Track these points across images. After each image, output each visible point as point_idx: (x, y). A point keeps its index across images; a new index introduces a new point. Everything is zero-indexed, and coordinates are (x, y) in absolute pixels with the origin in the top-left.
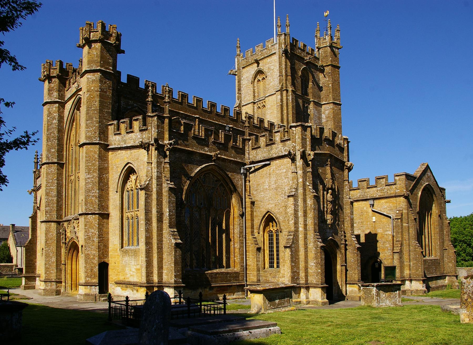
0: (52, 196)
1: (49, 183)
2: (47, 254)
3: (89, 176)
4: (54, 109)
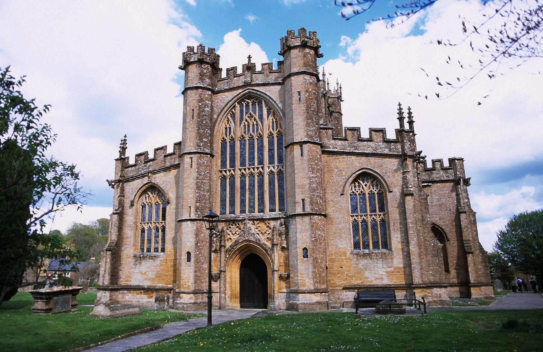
0: (204, 191)
1: (200, 175)
2: (197, 259)
3: (313, 175)
4: (207, 96)
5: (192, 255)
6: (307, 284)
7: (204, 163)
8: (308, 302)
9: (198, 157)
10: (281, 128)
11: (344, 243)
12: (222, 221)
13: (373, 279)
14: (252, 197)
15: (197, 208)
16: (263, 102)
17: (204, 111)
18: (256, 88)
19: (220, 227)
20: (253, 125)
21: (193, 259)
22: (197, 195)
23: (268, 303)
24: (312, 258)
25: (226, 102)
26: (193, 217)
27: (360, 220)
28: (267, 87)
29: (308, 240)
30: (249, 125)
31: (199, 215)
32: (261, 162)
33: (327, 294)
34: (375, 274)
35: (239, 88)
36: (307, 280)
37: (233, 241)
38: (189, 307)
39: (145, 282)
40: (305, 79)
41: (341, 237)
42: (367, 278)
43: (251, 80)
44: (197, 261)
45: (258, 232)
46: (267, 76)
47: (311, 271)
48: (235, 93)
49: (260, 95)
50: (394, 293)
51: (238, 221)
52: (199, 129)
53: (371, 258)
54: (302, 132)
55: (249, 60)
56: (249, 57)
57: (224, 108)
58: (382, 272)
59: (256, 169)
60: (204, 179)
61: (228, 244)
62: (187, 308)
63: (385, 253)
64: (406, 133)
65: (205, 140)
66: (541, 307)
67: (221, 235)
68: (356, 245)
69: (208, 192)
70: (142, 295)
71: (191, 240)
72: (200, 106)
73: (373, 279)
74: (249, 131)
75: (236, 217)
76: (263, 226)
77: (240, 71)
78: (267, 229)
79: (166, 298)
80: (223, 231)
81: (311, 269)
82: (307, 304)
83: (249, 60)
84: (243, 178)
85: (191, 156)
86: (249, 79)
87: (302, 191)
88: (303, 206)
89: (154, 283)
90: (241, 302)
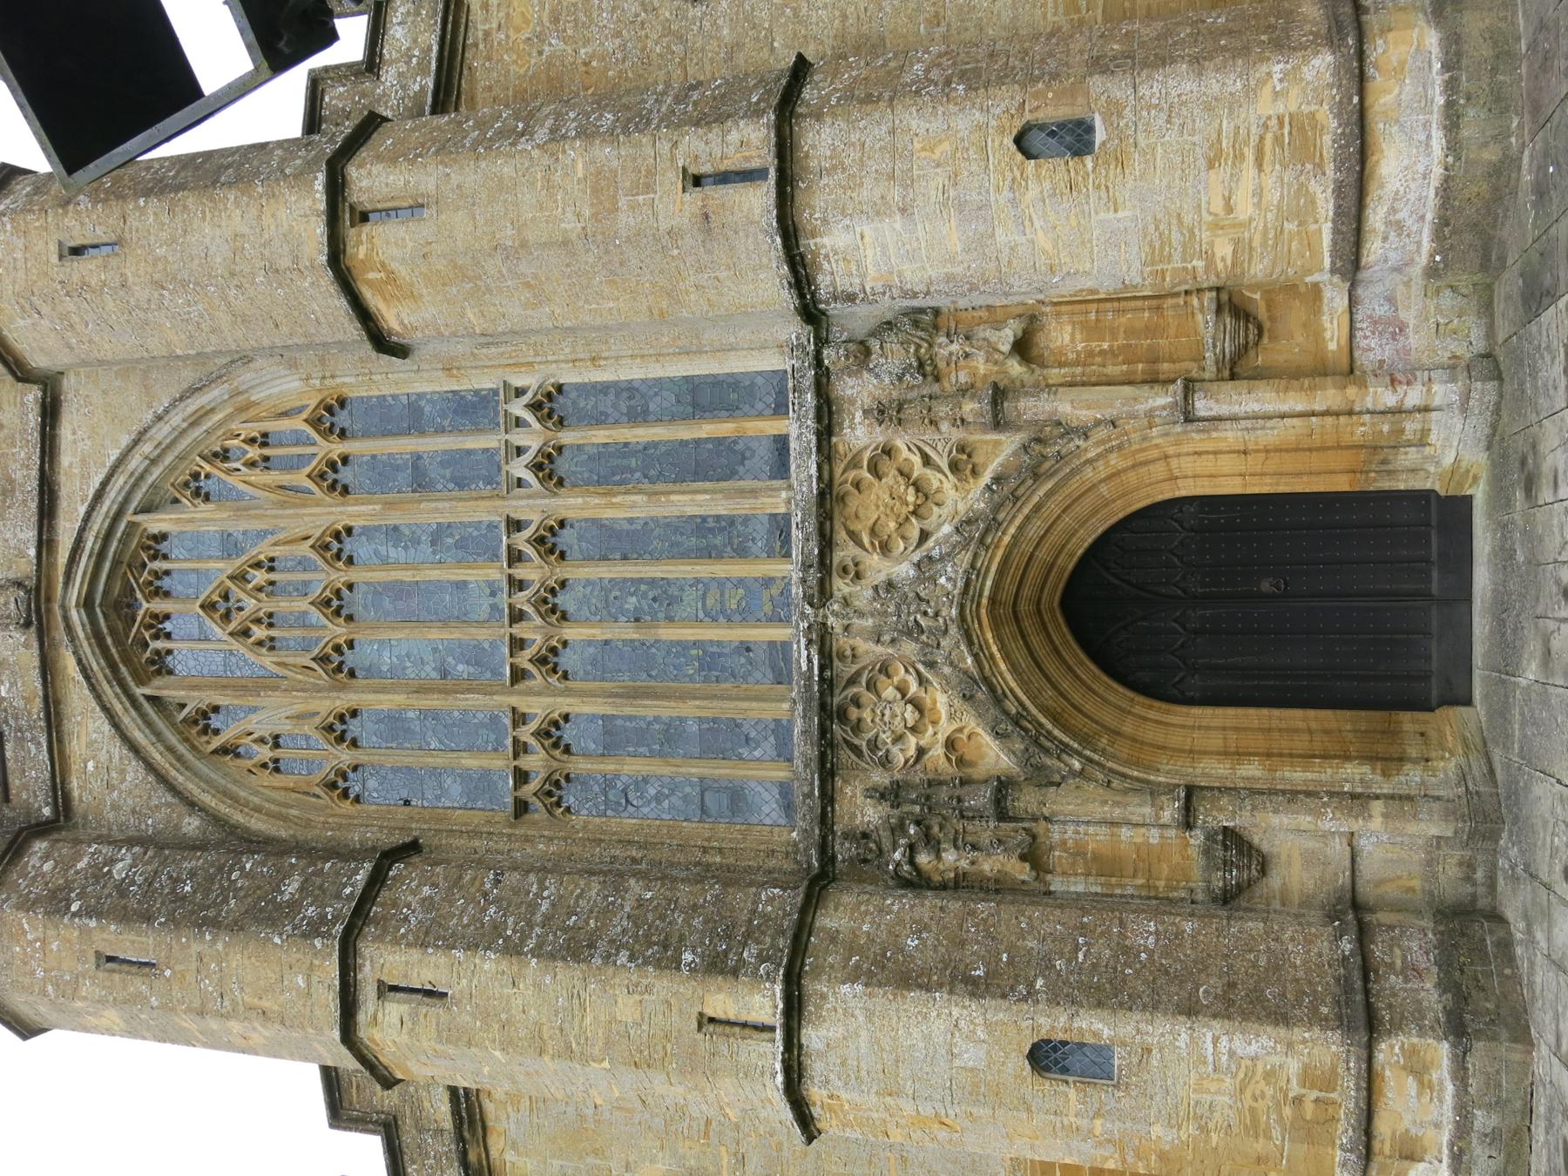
0: (606, 912)
1: (497, 928)
2: (1088, 989)
5: (1054, 1023)
6: (1293, 102)
7: (428, 904)
8: (1437, 79)
9: (379, 939)
10: (300, 410)
14: (690, 595)
15: (718, 966)
16: (155, 523)
17: (122, 890)
19: (871, 814)
21: (1093, 1025)
22: (623, 958)
23: (1426, 496)
24: (1096, 83)
25: (118, 750)
26: (765, 1004)
28: (64, 492)
29: (965, 121)
31: (762, 958)
36: (1266, 107)
37: (971, 723)
38: (1492, 1083)
44: (1107, 993)
45: (915, 534)
47: (1189, 86)
48: (77, 697)
51: (828, 685)
52: (214, 924)
54: (283, 214)
57: (150, 767)
59: (520, 572)
60: (533, 907)
61: (994, 755)
62: (1499, 1105)
65: (291, 887)
67: (926, 805)
69: (620, 889)
71: (939, 1027)
72: (88, 912)
75: (807, 702)
76: (874, 503)
80: (892, 794)
81: (1178, 83)
82: (1451, 86)
84: (566, 538)
85: (368, 993)
87: (634, 190)
88: (724, 178)
90: (1422, 705)
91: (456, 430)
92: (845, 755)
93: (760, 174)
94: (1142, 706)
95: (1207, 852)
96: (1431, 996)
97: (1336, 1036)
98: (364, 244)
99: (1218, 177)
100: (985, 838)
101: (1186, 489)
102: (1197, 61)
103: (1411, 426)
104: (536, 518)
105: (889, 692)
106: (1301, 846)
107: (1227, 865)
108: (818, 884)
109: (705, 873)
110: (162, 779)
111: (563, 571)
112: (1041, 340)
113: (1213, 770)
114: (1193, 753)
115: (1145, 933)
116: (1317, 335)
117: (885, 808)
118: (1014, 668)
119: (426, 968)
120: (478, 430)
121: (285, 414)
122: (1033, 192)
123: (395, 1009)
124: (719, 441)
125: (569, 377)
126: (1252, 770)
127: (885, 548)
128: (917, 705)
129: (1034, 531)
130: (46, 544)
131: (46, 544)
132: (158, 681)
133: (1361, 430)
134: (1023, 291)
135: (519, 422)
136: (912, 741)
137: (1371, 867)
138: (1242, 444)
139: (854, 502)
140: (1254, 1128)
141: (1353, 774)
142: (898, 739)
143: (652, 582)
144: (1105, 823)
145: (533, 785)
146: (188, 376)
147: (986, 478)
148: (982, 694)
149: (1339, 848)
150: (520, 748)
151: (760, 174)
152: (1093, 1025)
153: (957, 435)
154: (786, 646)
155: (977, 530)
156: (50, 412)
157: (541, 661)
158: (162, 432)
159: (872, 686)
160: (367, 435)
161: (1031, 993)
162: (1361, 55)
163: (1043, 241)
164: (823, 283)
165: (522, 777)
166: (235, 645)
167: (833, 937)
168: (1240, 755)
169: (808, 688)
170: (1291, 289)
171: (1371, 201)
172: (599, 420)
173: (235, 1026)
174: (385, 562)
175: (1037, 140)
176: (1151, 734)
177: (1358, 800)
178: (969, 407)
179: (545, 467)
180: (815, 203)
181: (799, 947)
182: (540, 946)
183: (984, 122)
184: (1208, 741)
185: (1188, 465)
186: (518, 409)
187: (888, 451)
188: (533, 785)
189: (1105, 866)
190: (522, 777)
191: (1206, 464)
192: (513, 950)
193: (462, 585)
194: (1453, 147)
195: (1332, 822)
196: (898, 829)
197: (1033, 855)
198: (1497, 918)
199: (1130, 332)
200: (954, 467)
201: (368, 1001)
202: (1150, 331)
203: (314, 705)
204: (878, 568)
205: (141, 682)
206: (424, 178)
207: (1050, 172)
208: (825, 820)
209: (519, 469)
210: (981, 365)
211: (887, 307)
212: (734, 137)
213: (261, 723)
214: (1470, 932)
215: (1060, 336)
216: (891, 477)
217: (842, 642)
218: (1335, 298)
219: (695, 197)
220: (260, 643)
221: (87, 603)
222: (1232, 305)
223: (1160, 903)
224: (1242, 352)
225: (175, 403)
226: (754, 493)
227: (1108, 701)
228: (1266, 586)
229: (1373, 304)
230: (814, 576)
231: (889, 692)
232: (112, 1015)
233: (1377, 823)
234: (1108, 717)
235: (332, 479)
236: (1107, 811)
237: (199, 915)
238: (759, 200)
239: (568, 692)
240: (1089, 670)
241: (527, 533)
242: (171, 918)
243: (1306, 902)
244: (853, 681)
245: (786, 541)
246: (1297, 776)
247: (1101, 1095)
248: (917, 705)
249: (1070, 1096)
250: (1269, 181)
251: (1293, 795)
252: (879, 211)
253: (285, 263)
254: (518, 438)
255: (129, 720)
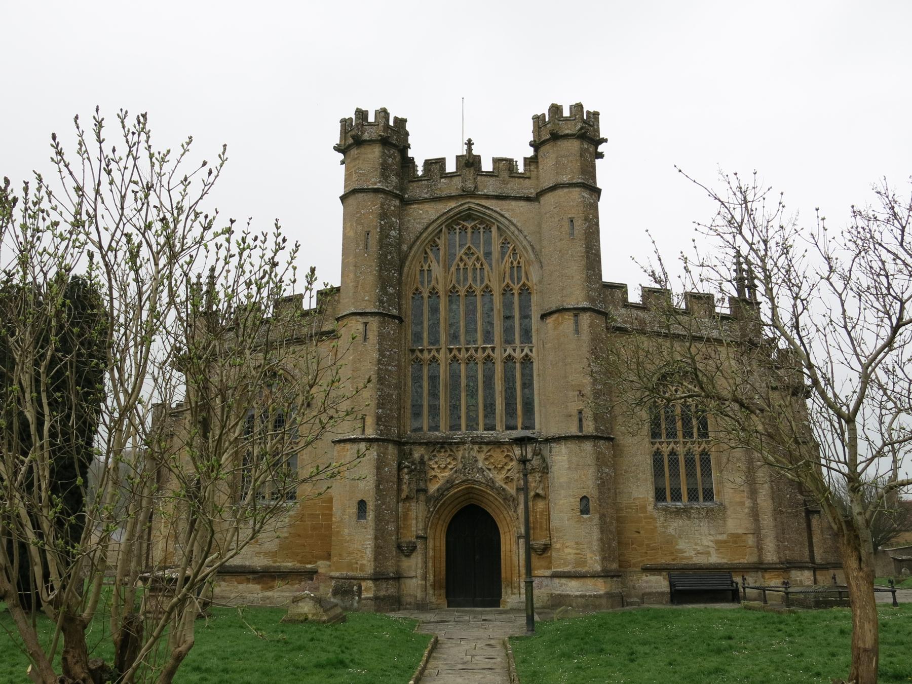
0: (389, 386)
5: (371, 506)
8: (592, 594)
9: (380, 322)
10: (528, 279)
11: (640, 490)
12: (420, 444)
13: (693, 554)
14: (473, 402)
15: (379, 419)
16: (494, 229)
17: (388, 236)
18: (484, 202)
20: (475, 269)
21: (371, 515)
22: (379, 393)
24: (597, 516)
25: (426, 222)
26: (370, 433)
27: (666, 450)
30: (465, 269)
32: (488, 336)
33: (619, 579)
34: (696, 544)
35: (450, 198)
36: (589, 555)
37: (441, 482)
39: (255, 559)
40: (584, 197)
41: (638, 479)
42: (683, 552)
43: (476, 187)
44: (378, 519)
45: (490, 467)
46: (505, 182)
49: (490, 216)
50: (731, 577)
51: (450, 444)
52: (381, 269)
53: (689, 518)
54: (578, 292)
55: (470, 150)
56: (470, 143)
57: (421, 234)
58: (707, 541)
59: (480, 351)
61: (433, 488)
63: (712, 510)
64: (744, 304)
65: (391, 290)
66: (910, 600)
67: (420, 471)
68: (660, 495)
70: (250, 585)
72: (381, 227)
73: (693, 554)
74: (466, 279)
75: (445, 438)
76: (498, 456)
77: (451, 167)
78: (507, 460)
79: (355, 588)
80: (422, 462)
81: (596, 534)
82: (590, 596)
83: (470, 150)
84: (490, 365)
85: (365, 319)
86: (470, 185)
88: (580, 420)
89: (275, 562)
91: (521, 330)
92: (431, 449)
93: (581, 431)
94: (446, 525)
95: (410, 542)
96: (382, 593)
97: (372, 571)
98: (569, 318)
99: (572, 544)
100: (412, 486)
101: (502, 536)
102: (601, 539)
103: (516, 591)
104: (495, 356)
105: (448, 460)
106: (414, 565)
107: (408, 547)
108: (399, 444)
109: (399, 414)
110: (418, 238)
111: (480, 363)
112: (540, 500)
113: (431, 544)
114: (434, 539)
115: (391, 527)
116: (539, 569)
117: (418, 460)
118: (455, 493)
119: (373, 337)
120: (521, 336)
121: (527, 274)
122: (572, 500)
123: (361, 327)
124: (516, 410)
125: (535, 366)
126: (431, 553)
127: (486, 459)
128: (446, 467)
129: (490, 498)
130: (487, 197)
131: (487, 197)
132: (446, 231)
133: (515, 579)
134: (551, 496)
135: (522, 351)
136: (436, 466)
137: (408, 581)
138: (512, 550)
139: (498, 450)
140: (350, 553)
141: (431, 577)
142: (436, 463)
143: (477, 390)
144: (417, 517)
145: (419, 355)
146: (537, 247)
147: (504, 486)
148: (449, 485)
149: (413, 574)
150: (430, 351)
151: (581, 431)
152: (371, 515)
153: (515, 478)
154: (460, 429)
155: (491, 483)
156: (528, 199)
157: (455, 357)
158: (521, 238)
159: (450, 455)
160: (520, 301)
161: (377, 500)
162: (599, 577)
163: (561, 502)
164: (554, 445)
165: (422, 351)
166: (458, 258)
167: (387, 449)
168: (434, 550)
169: (449, 438)
170: (550, 562)
171: (568, 580)
172: (523, 375)
173: (352, 276)
174: (483, 306)
175: (584, 502)
176: (439, 528)
177: (425, 578)
178: (522, 482)
179: (510, 358)
180: (573, 446)
181: (383, 441)
182: (381, 369)
183: (591, 490)
184: (438, 542)
185: (508, 538)
186: (526, 350)
187: (512, 460)
188: (419, 355)
189: (406, 517)
190: (422, 351)
191: (508, 542)
192: (379, 362)
193: (476, 331)
194: (576, 597)
195: (420, 572)
196: (413, 463)
197: (408, 498)
198: (399, 610)
199: (541, 523)
200: (507, 478)
201: (362, 319)
202: (541, 527)
203: (440, 284)
204: (481, 457)
205: (446, 226)
206: (585, 336)
207: (576, 504)
208: (414, 443)
209: (509, 351)
210: (533, 485)
211: (548, 460)
212: (590, 423)
213: (434, 266)
214: (396, 602)
215: (541, 505)
216: (505, 460)
217: (462, 448)
218: (548, 573)
219: (575, 412)
220: (458, 265)
221: (470, 209)
222: (547, 548)
223: (398, 529)
224: (535, 550)
225: (529, 242)
226: (501, 421)
227: (447, 517)
228: (477, 557)
229: (546, 582)
230: (479, 440)
231: (448, 460)
232: (351, 234)
233: (420, 582)
234: (443, 517)
235: (507, 291)
236: (420, 515)
237: (383, 263)
238: (574, 430)
239: (446, 365)
240: (455, 511)
241: (491, 353)
242: (382, 255)
243: (399, 566)
244: (451, 450)
245: (488, 429)
246: (430, 564)
247: (355, 517)
248: (446, 467)
249: (354, 510)
250: (572, 556)
251: (426, 563)
252: (570, 462)
253: (565, 293)
254: (518, 350)
255: (435, 225)
